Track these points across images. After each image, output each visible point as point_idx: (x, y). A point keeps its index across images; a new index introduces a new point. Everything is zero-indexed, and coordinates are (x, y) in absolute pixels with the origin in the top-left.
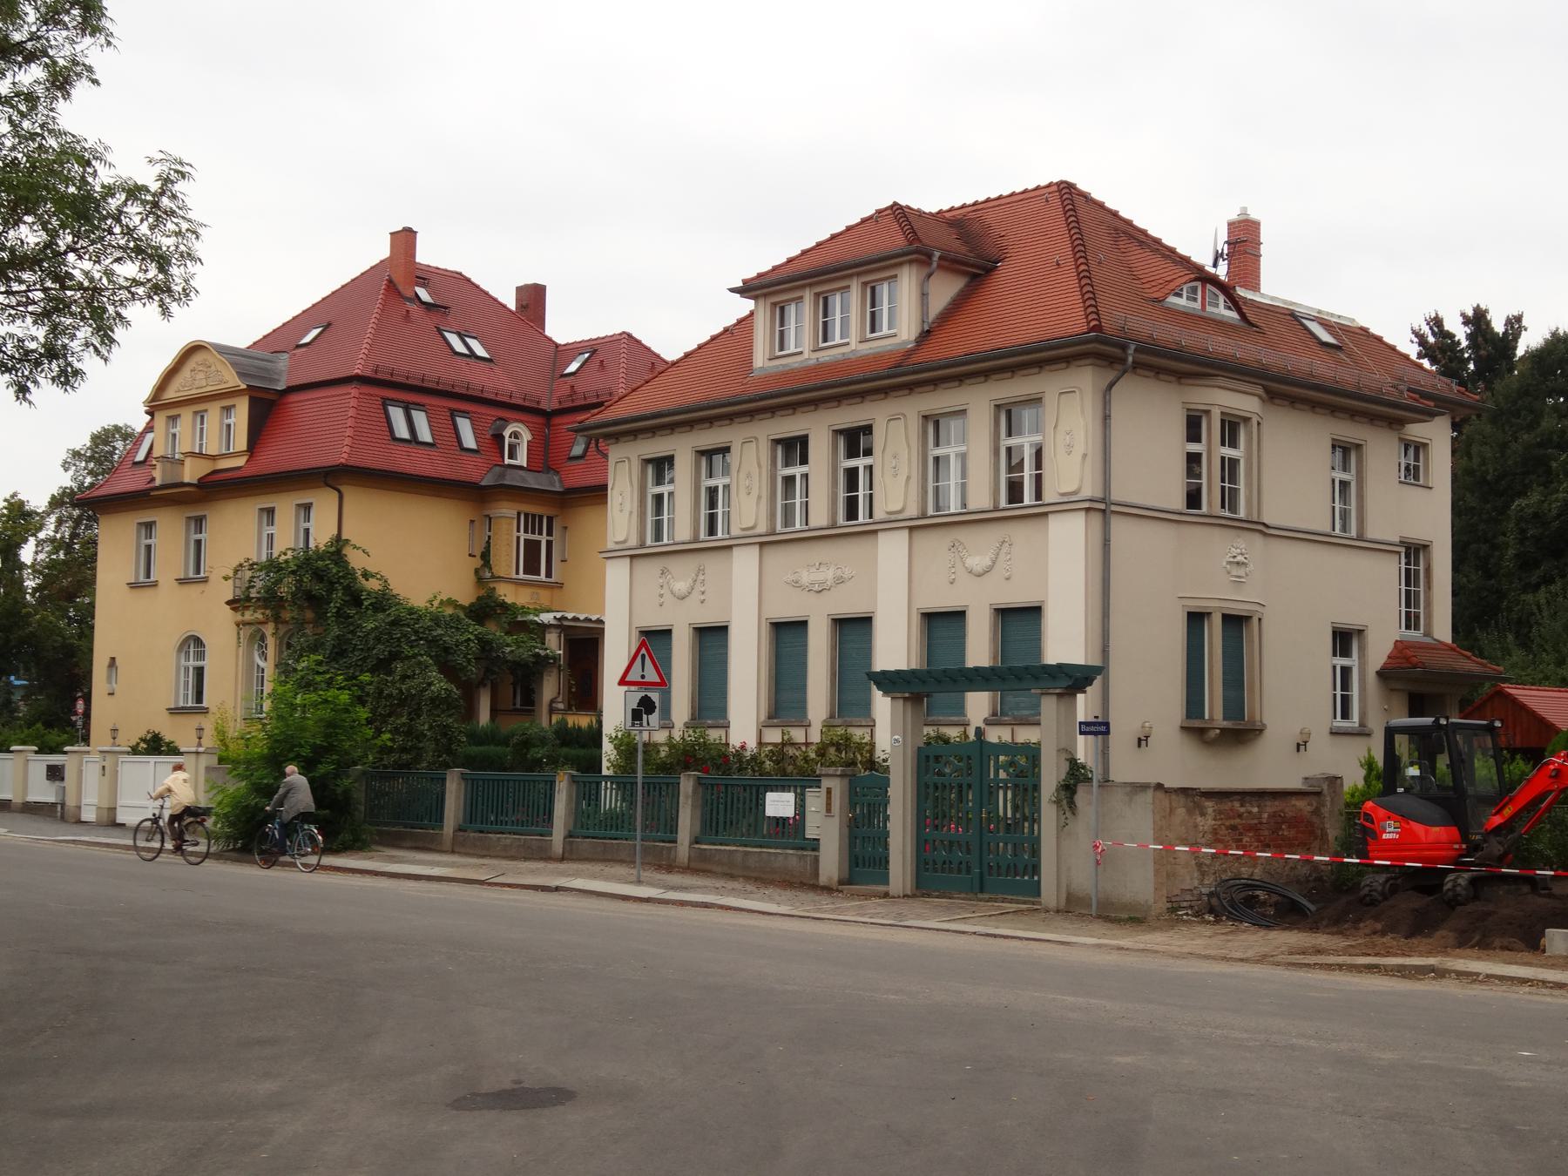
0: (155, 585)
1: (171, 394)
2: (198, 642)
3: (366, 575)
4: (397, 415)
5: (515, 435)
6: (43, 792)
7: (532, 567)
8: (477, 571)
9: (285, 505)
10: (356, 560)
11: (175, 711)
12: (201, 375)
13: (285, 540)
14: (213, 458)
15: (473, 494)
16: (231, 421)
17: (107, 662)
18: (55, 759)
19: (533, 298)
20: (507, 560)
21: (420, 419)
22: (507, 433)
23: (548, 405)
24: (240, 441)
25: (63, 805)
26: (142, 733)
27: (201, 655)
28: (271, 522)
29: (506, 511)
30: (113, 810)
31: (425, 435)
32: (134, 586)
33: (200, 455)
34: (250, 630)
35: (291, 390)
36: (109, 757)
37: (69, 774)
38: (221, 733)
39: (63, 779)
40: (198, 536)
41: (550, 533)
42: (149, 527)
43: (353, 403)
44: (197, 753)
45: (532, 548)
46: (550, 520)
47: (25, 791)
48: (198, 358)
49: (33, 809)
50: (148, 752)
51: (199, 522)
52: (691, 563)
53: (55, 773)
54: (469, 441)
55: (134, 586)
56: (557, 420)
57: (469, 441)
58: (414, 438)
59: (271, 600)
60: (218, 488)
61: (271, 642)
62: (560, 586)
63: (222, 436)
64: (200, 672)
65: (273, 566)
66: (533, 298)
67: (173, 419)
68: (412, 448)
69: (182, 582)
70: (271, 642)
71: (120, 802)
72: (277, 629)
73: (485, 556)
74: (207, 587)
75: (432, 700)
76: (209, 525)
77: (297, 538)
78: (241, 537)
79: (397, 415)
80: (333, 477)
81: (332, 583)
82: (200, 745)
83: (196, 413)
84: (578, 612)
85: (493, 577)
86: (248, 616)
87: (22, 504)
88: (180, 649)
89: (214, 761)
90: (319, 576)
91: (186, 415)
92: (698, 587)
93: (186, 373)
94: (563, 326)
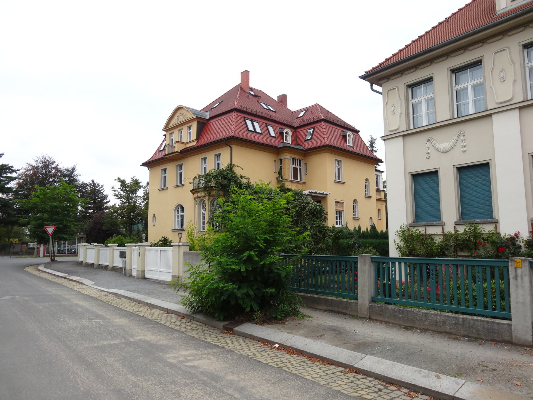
0: (167, 189)
1: (171, 125)
2: (182, 207)
3: (241, 177)
4: (249, 123)
5: (287, 133)
6: (118, 263)
7: (295, 177)
8: (277, 178)
9: (210, 156)
10: (238, 172)
11: (174, 231)
12: (181, 117)
13: (211, 166)
14: (185, 144)
15: (275, 150)
16: (191, 131)
17: (152, 215)
18: (122, 249)
19: (283, 99)
20: (288, 174)
21: (256, 124)
22: (284, 132)
23: (296, 125)
24: (194, 136)
25: (125, 268)
26: (160, 238)
27: (182, 211)
28: (205, 163)
29: (287, 157)
30: (143, 272)
31: (258, 130)
32: (160, 190)
33: (181, 142)
34: (198, 200)
35: (212, 118)
36: (141, 248)
37: (128, 255)
38: (190, 235)
39: (125, 257)
40: (181, 171)
41: (300, 166)
42: (165, 170)
43: (234, 117)
44: (179, 245)
45: (295, 170)
46: (300, 161)
47: (113, 262)
48: (180, 111)
49: (115, 269)
50: (162, 245)
51: (181, 166)
52: (454, 131)
53: (123, 255)
54: (273, 134)
55: (160, 190)
56: (298, 130)
57: (273, 134)
58: (255, 131)
59: (207, 189)
60: (188, 153)
61: (207, 203)
62: (305, 183)
63: (189, 136)
64: (182, 217)
65: (207, 176)
66: (283, 99)
67: (172, 134)
68: (255, 134)
69: (176, 187)
70: (207, 203)
71: (146, 268)
72: (209, 198)
73: (280, 173)
74: (184, 187)
75: (310, 211)
76: (184, 167)
77: (215, 166)
78: (194, 168)
79: (249, 123)
80: (228, 141)
81: (230, 180)
82: (180, 241)
83: (179, 130)
84: (318, 190)
85: (283, 180)
86: (199, 194)
87: (136, 180)
88: (175, 210)
89: (187, 249)
90: (224, 177)
91: (176, 131)
92: (460, 144)
93: (176, 118)
94: (293, 105)
